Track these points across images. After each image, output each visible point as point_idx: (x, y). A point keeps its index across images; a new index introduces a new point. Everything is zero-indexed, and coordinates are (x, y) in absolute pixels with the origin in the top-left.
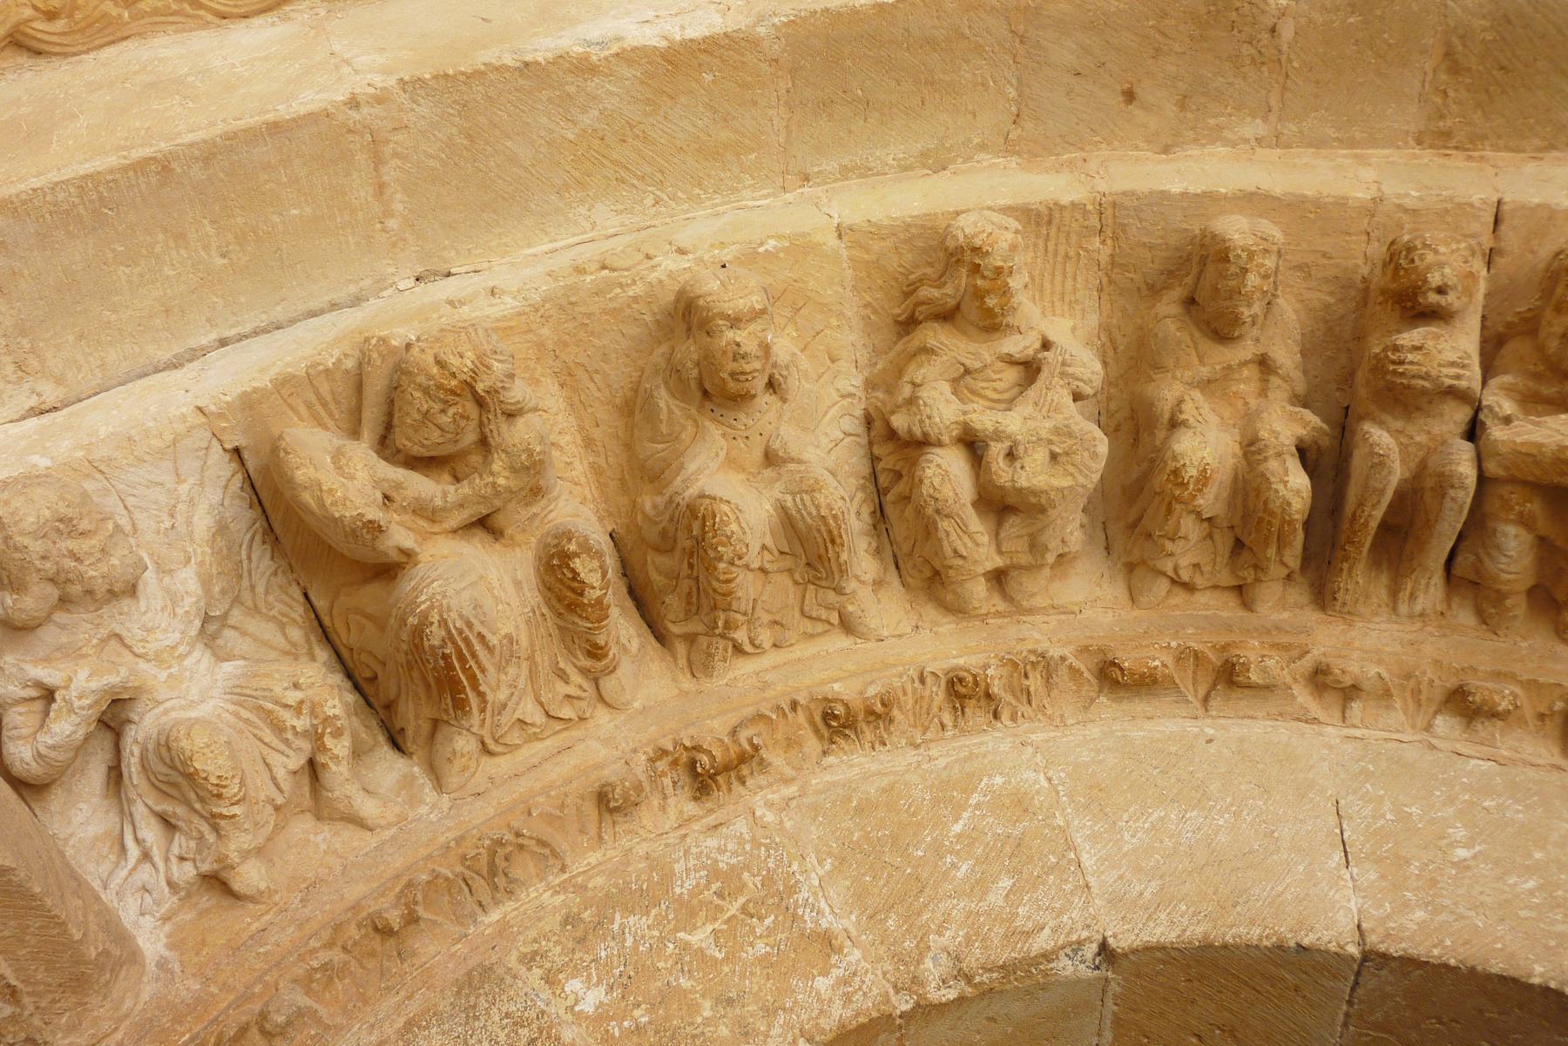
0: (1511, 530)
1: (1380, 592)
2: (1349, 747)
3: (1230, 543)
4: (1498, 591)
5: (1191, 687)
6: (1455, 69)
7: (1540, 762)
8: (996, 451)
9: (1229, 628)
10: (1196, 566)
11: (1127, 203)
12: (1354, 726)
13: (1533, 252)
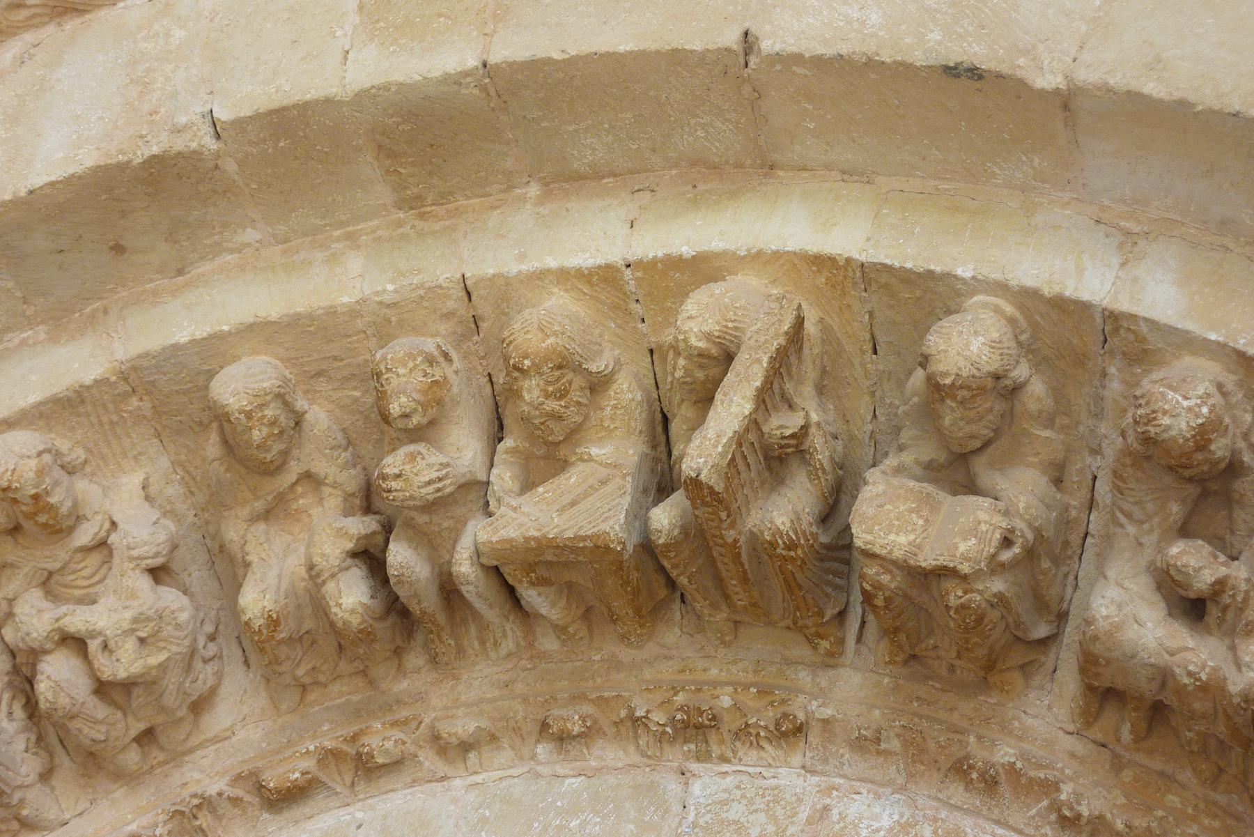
2: (472, 796)
5: (338, 779)
6: (392, 155)
7: (620, 765)
8: (94, 645)
11: (145, 363)
12: (476, 773)
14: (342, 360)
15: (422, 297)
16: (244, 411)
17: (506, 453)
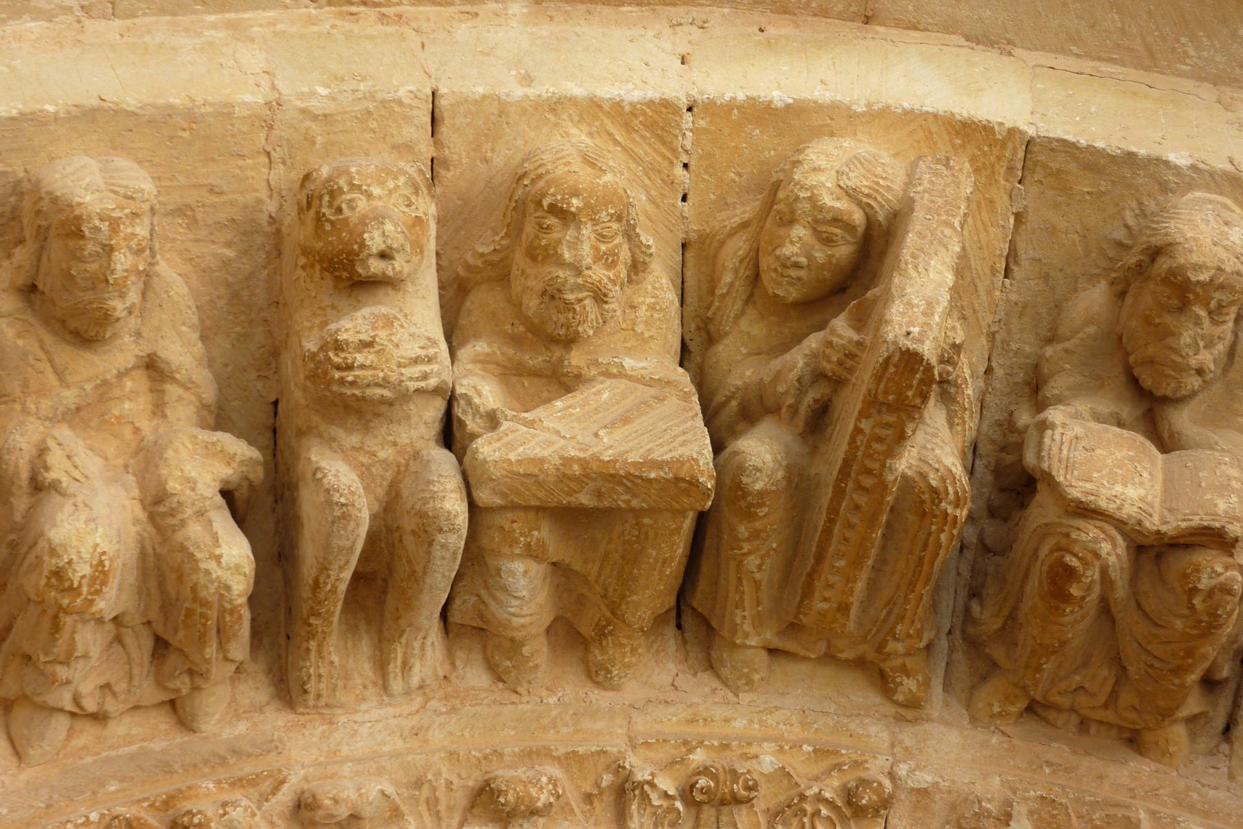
0: (519, 566)
1: (364, 669)
3: (148, 644)
4: (512, 640)
9: (166, 769)
10: (106, 687)
13: (486, 160)
14: (222, 193)
15: (369, 113)
16: (110, 218)
17: (475, 362)
